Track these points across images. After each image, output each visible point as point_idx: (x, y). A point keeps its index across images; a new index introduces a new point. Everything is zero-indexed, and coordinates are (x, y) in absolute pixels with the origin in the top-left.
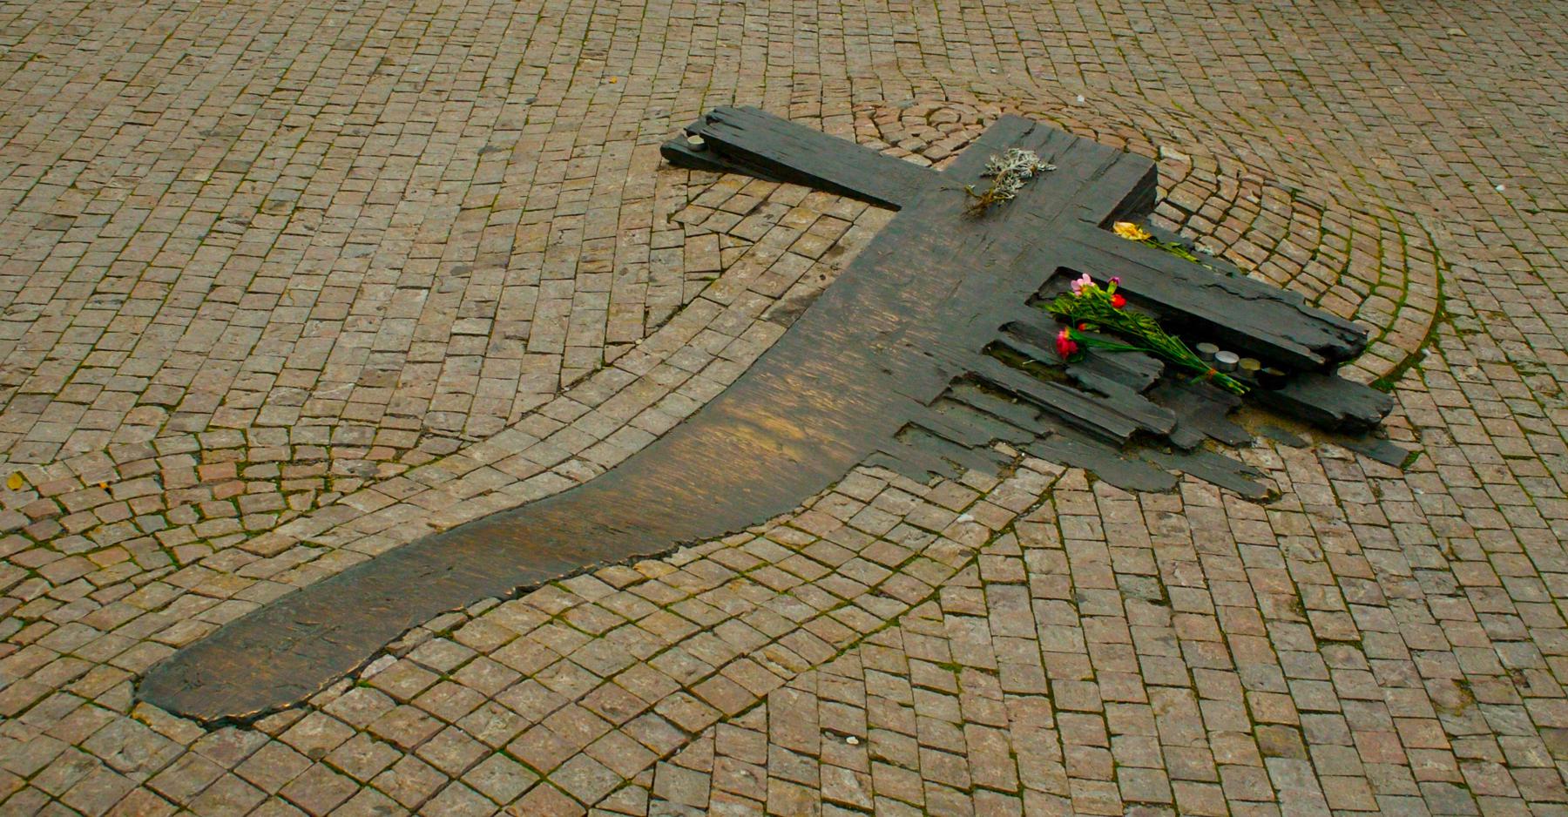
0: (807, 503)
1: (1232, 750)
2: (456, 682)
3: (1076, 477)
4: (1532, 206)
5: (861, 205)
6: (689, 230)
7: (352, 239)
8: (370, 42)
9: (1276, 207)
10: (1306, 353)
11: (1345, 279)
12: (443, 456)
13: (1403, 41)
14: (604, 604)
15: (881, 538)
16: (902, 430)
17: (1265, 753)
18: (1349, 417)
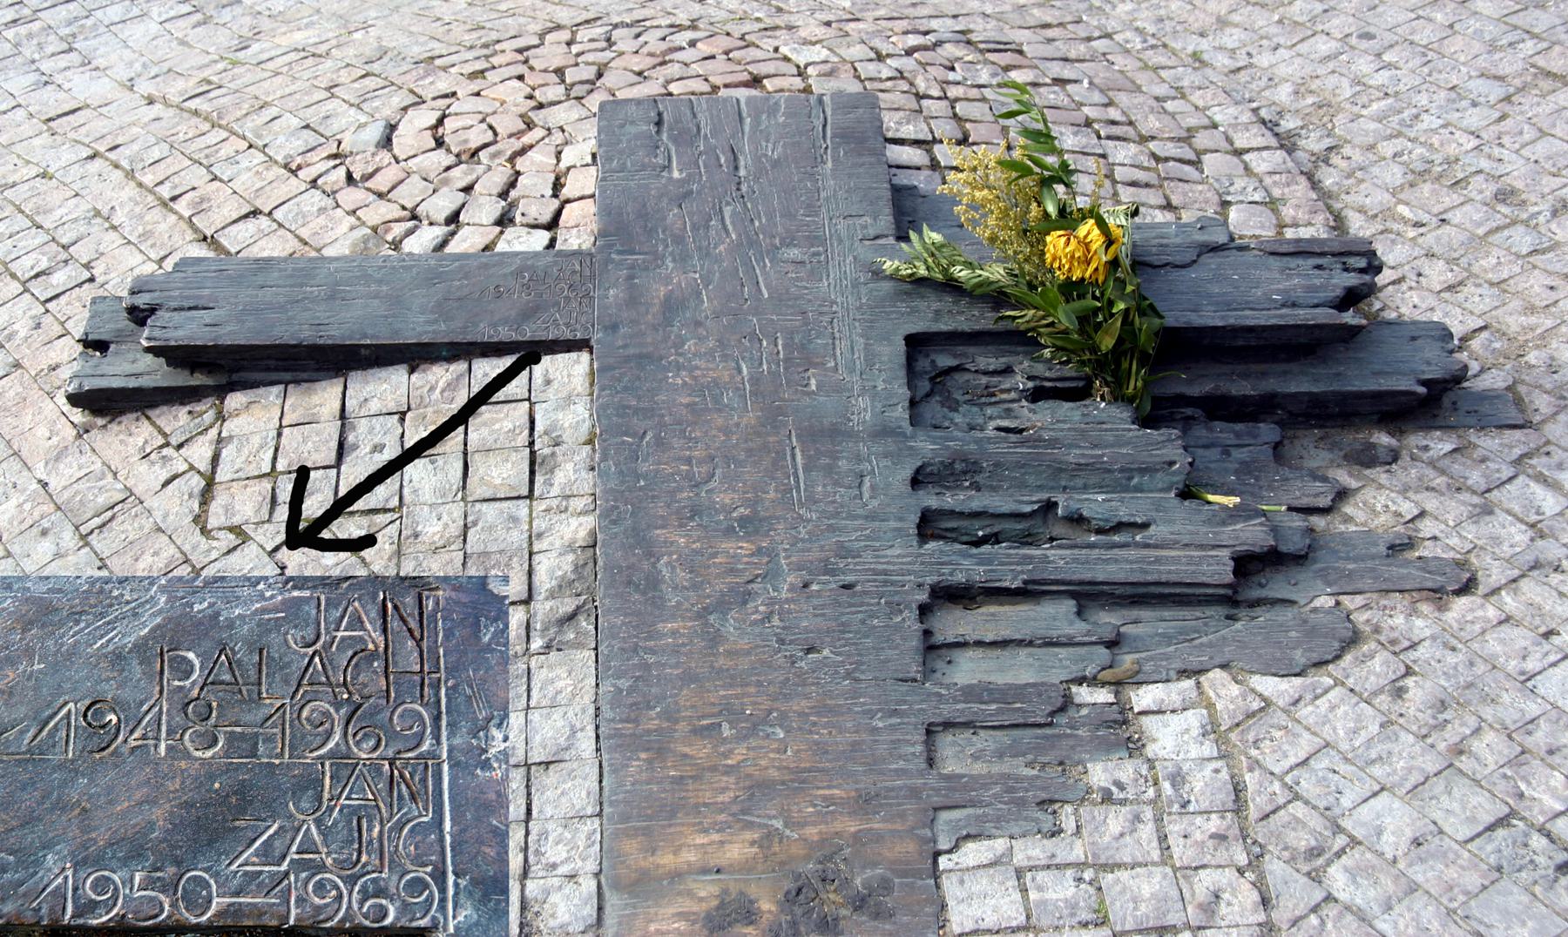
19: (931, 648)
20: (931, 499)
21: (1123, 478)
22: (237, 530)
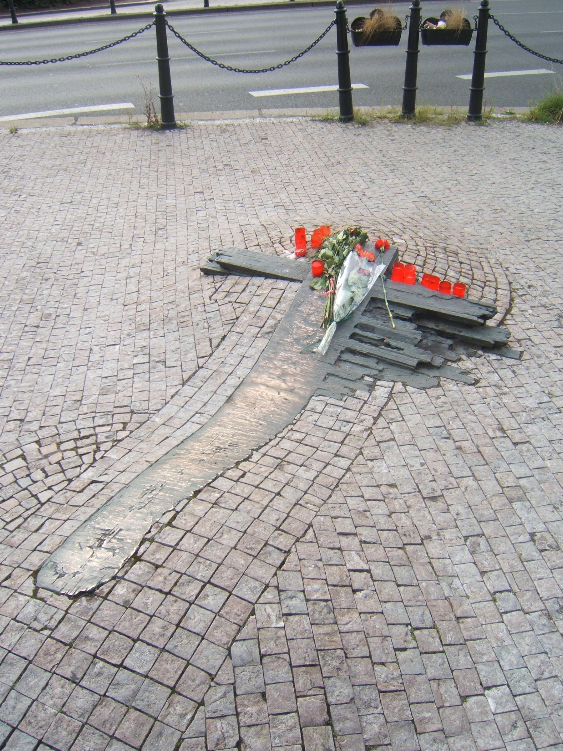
0: (297, 418)
1: (497, 503)
2: (180, 550)
3: (399, 387)
4: (527, 239)
5: (286, 282)
6: (220, 302)
7: (82, 327)
8: (71, 236)
9: (441, 256)
10: (475, 319)
11: (475, 282)
12: (144, 423)
13: (459, 178)
14: (233, 492)
15: (330, 429)
16: (325, 378)
17: (511, 501)
18: (496, 342)
19: (339, 360)
20: (357, 331)
21: (403, 338)
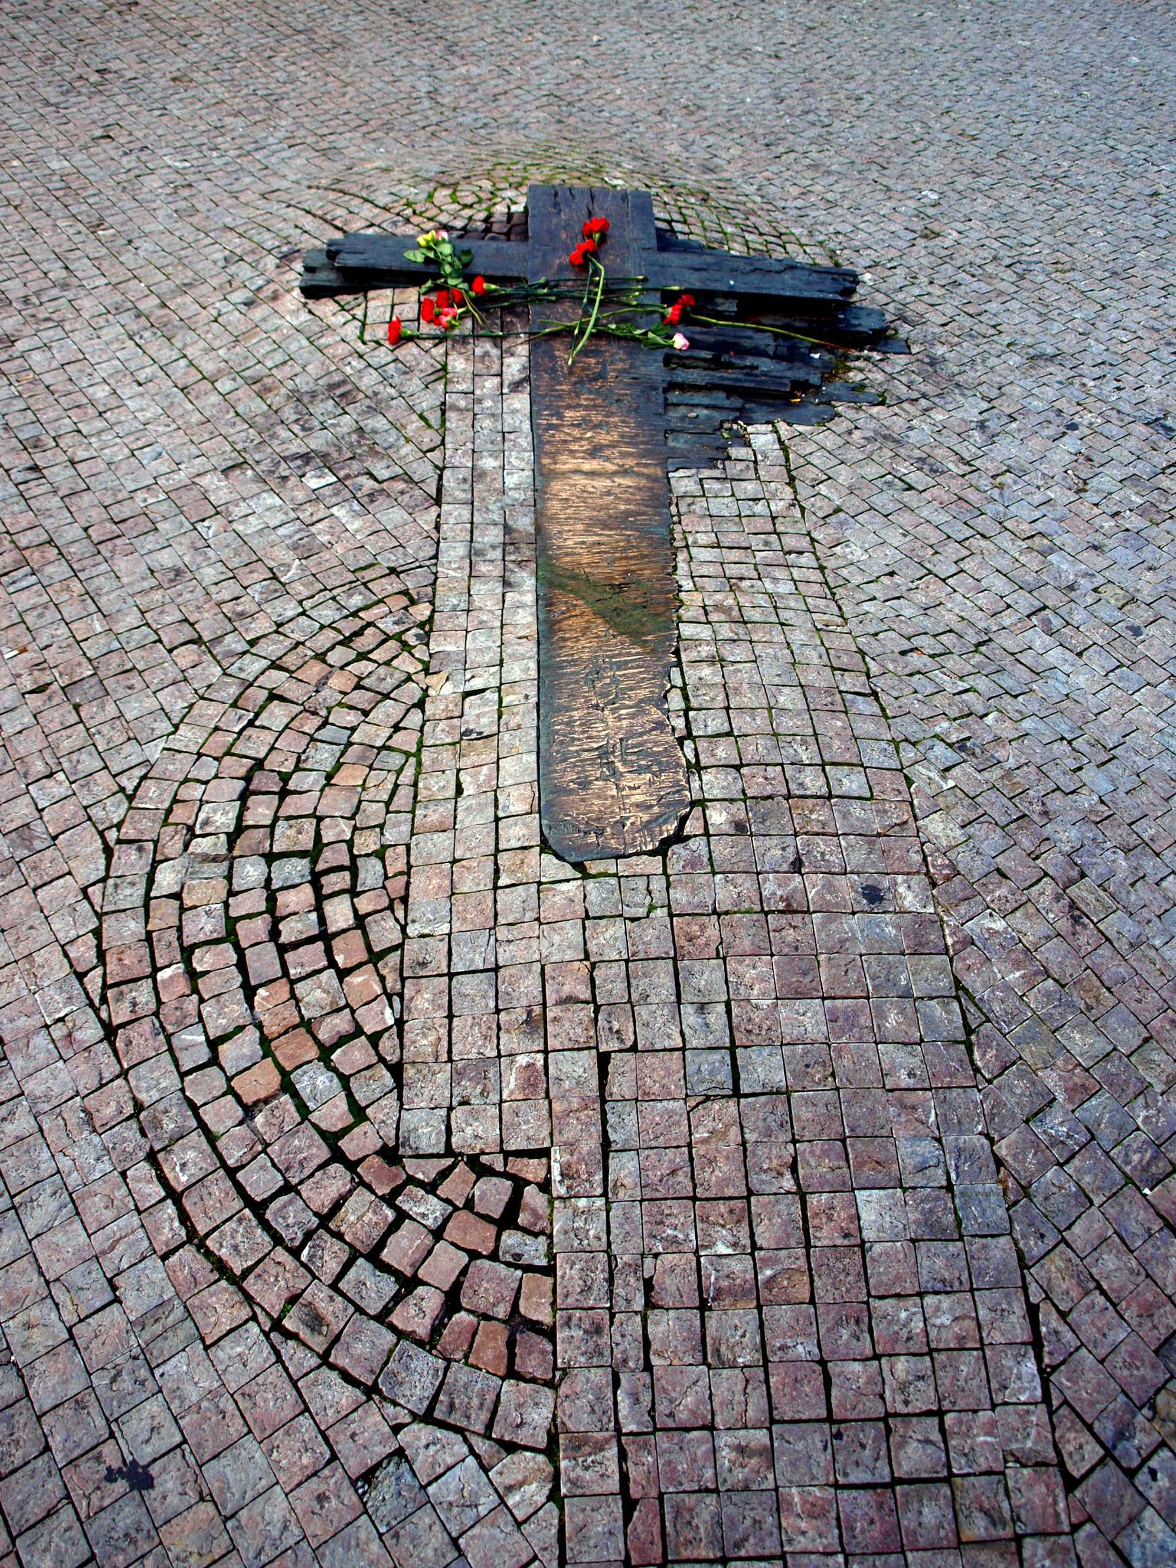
22: (377, 342)
